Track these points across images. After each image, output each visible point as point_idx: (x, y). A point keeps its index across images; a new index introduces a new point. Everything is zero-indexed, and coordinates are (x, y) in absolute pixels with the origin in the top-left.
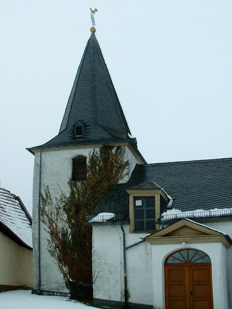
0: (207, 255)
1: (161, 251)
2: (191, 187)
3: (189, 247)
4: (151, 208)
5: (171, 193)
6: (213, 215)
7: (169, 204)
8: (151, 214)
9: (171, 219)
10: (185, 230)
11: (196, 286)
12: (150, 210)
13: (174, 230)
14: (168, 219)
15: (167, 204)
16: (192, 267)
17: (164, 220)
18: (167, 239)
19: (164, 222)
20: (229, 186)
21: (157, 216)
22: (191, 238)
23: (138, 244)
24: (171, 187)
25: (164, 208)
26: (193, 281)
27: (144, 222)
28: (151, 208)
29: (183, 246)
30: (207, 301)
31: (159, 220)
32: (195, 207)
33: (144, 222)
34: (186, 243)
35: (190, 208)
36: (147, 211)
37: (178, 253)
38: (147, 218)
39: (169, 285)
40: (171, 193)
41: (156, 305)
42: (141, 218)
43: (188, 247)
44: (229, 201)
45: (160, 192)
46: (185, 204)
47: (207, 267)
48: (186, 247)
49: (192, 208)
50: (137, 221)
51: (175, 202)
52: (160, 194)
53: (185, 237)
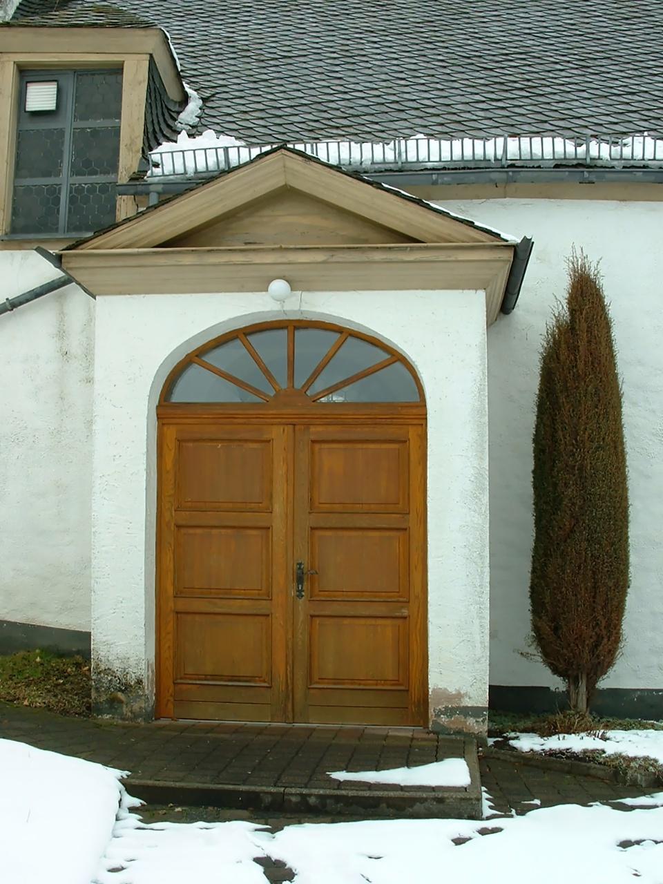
0: (396, 357)
1: (145, 330)
2: (285, 57)
3: (305, 308)
4: (99, 123)
5: (194, 76)
6: (412, 157)
7: (183, 116)
8: (99, 149)
9: (196, 172)
10: (288, 218)
11: (329, 533)
12: (95, 132)
13: (226, 210)
14: (186, 173)
15: (174, 115)
16: (313, 429)
17: (164, 175)
18: (186, 258)
19: (160, 188)
20: (456, 57)
21: (128, 161)
22: (320, 257)
23: (21, 303)
24: (193, 55)
25: (161, 125)
26: (312, 507)
27: (59, 193)
28: (99, 123)
29: (273, 300)
30: (388, 622)
31: (138, 177)
32: (310, 131)
33: (60, 189)
34: (294, 284)
35: (284, 133)
36: (79, 134)
37: (195, 371)
38: (76, 171)
39: (179, 527)
40: (194, 76)
41: (106, 644)
42: (47, 174)
43: (296, 308)
44: (469, 112)
45: (149, 42)
46: (262, 119)
47: (396, 421)
48: (287, 307)
49: (298, 136)
50: (28, 190)
51: (212, 108)
52: (151, 55)
53: (287, 249)
